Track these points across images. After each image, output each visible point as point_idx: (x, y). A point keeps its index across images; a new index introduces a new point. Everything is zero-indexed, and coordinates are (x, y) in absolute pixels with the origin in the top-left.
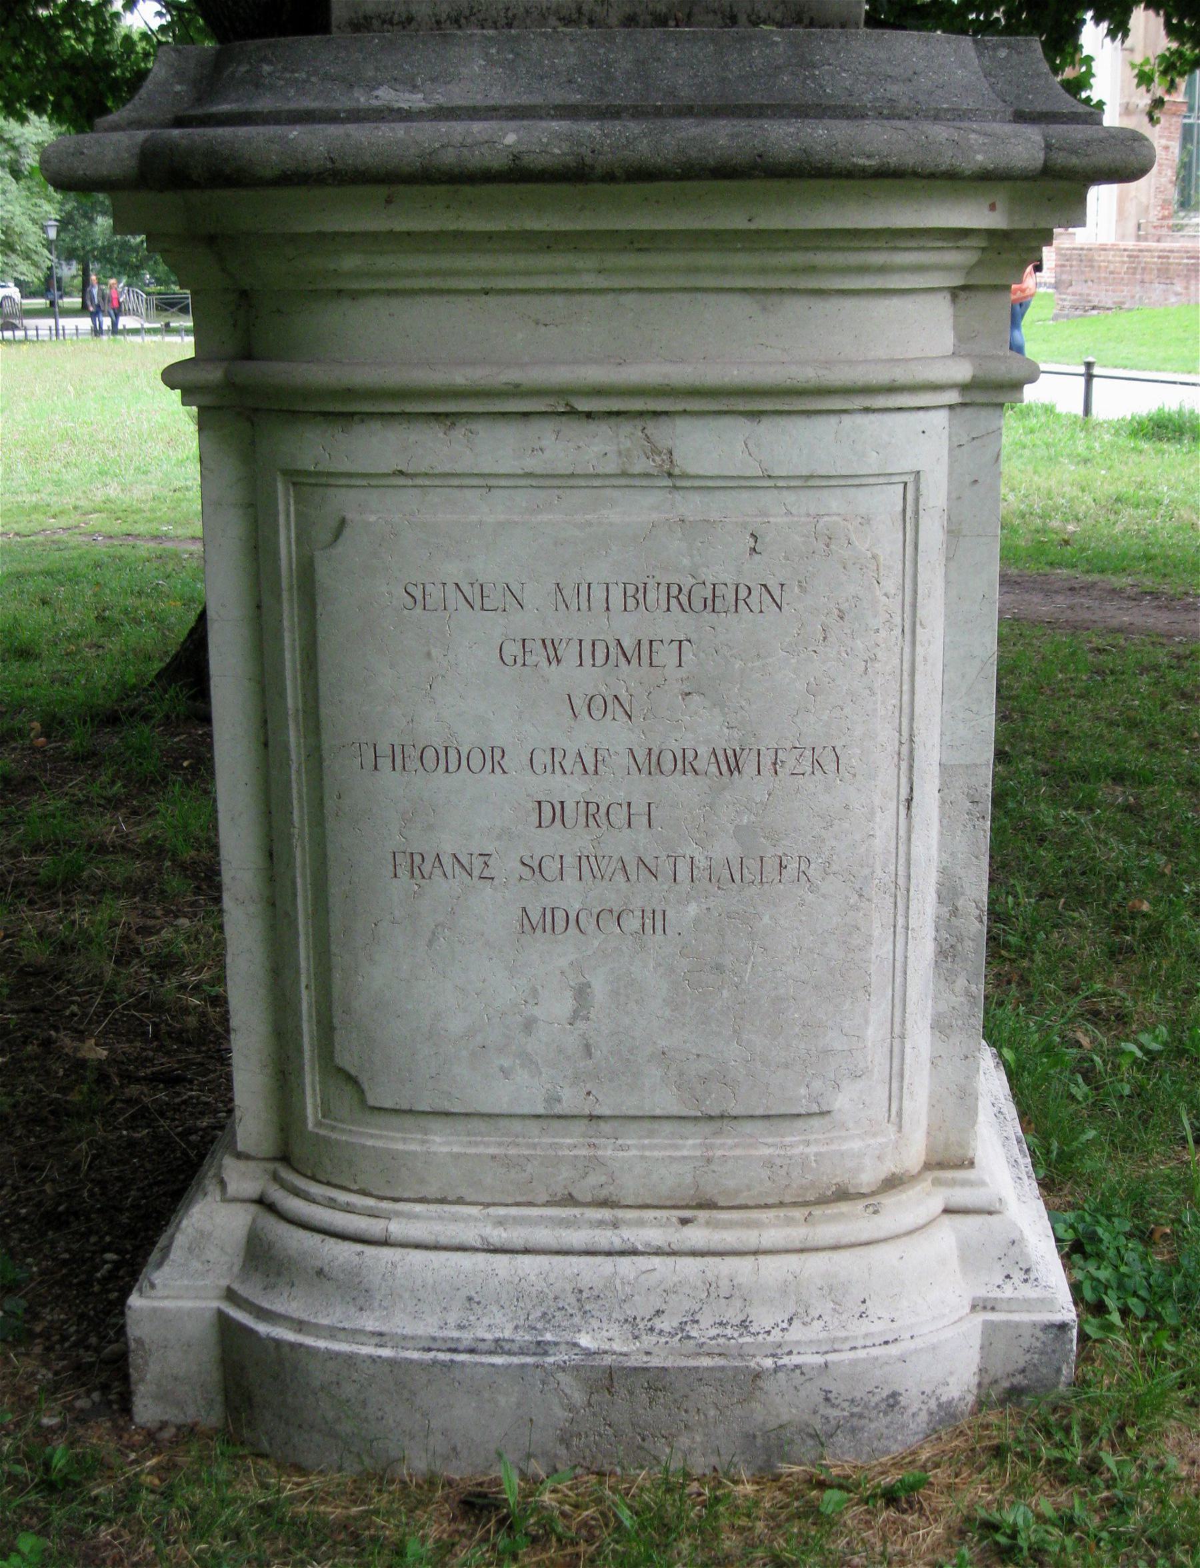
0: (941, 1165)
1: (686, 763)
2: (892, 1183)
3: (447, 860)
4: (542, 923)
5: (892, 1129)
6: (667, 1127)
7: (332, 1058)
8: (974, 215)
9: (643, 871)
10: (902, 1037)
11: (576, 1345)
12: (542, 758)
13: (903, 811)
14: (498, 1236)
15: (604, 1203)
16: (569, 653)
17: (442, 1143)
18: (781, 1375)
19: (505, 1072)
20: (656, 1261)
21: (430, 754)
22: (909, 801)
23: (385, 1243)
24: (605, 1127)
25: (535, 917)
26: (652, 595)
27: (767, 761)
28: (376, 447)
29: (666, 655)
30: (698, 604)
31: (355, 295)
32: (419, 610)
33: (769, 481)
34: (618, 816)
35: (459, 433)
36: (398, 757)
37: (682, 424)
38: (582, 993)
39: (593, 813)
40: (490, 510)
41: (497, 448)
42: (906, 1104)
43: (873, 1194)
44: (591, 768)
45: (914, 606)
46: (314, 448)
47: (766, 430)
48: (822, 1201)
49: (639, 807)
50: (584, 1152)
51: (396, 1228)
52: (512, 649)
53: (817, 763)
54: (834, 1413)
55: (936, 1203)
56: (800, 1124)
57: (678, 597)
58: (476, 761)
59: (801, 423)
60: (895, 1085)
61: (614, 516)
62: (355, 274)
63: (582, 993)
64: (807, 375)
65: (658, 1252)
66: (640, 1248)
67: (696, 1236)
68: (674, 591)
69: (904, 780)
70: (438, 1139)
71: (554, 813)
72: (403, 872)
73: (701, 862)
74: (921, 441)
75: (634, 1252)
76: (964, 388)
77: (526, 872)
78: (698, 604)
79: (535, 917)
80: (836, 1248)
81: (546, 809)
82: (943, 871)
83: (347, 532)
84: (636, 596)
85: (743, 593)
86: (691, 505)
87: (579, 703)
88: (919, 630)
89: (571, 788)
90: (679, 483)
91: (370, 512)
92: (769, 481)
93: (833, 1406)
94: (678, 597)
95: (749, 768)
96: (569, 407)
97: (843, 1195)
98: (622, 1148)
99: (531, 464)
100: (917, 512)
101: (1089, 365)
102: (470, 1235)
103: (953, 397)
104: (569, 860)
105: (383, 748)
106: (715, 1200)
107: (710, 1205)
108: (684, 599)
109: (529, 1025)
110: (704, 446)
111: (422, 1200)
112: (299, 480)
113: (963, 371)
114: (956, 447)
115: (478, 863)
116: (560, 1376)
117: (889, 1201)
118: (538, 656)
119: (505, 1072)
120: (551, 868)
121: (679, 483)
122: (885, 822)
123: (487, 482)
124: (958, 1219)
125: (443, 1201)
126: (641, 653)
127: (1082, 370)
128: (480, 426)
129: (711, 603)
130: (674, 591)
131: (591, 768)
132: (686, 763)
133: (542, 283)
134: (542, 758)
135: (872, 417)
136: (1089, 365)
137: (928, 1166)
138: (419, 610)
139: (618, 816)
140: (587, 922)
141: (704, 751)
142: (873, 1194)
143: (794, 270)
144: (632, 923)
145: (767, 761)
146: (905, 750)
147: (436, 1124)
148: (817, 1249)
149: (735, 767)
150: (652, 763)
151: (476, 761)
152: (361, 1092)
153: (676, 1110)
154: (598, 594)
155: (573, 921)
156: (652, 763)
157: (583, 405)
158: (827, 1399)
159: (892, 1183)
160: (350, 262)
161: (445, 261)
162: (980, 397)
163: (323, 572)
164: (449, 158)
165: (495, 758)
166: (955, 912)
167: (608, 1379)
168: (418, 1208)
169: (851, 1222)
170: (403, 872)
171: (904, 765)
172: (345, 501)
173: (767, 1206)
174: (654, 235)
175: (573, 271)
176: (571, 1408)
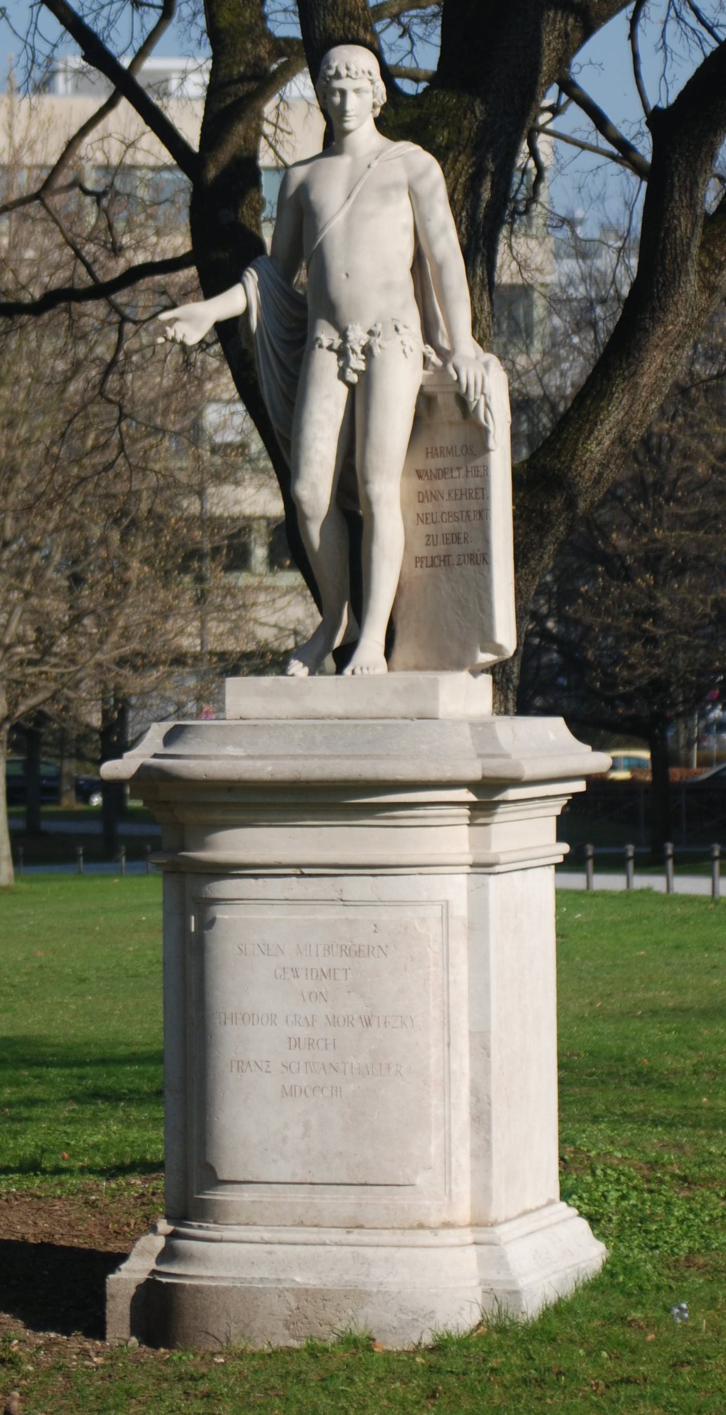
0: (477, 1225)
1: (348, 1021)
2: (447, 1225)
3: (252, 1063)
4: (288, 1092)
5: (446, 1199)
9: (332, 1070)
10: (450, 1154)
11: (294, 1281)
12: (291, 1019)
13: (446, 1048)
14: (267, 1236)
15: (316, 1226)
16: (302, 973)
18: (380, 1296)
19: (275, 1161)
20: (334, 1248)
21: (246, 1017)
22: (449, 1044)
23: (221, 1241)
25: (288, 1089)
26: (335, 949)
27: (382, 1021)
29: (340, 975)
30: (353, 953)
32: (243, 956)
34: (322, 1044)
38: (307, 1126)
39: (311, 1043)
40: (271, 914)
42: (453, 1187)
43: (436, 1228)
44: (310, 1023)
45: (448, 958)
48: (411, 1228)
49: (330, 1041)
50: (308, 1201)
52: (279, 972)
53: (403, 1023)
54: (404, 1317)
55: (470, 1239)
57: (346, 951)
58: (265, 1020)
60: (447, 1178)
61: (319, 917)
63: (307, 1126)
64: (393, 860)
65: (336, 1244)
66: (328, 1242)
67: (355, 1236)
68: (344, 948)
69: (446, 1034)
70: (247, 1195)
71: (294, 1043)
72: (235, 1069)
73: (356, 1066)
74: (456, 888)
75: (325, 1244)
76: (472, 866)
77: (284, 1069)
78: (353, 953)
79: (288, 1089)
80: (412, 1247)
81: (292, 1040)
82: (472, 1081)
84: (328, 949)
85: (371, 949)
86: (350, 913)
87: (306, 995)
88: (451, 969)
89: (302, 1032)
90: (346, 903)
91: (222, 914)
93: (404, 1313)
94: (346, 951)
97: (421, 1226)
98: (324, 1199)
100: (447, 918)
102: (256, 1236)
104: (302, 1064)
106: (364, 1224)
107: (361, 1227)
108: (347, 951)
110: (356, 887)
111: (239, 1224)
113: (470, 859)
114: (470, 891)
115: (265, 1064)
116: (286, 1293)
117: (443, 1233)
118: (289, 975)
119: (275, 1161)
120: (294, 1067)
121: (346, 903)
122: (435, 1053)
124: (479, 1247)
125: (247, 1224)
126: (328, 974)
129: (358, 953)
130: (344, 948)
131: (310, 1023)
132: (348, 1021)
134: (291, 1019)
135: (423, 877)
137: (471, 1225)
138: (243, 956)
139: (322, 1044)
140: (309, 1092)
141: (356, 1016)
142: (436, 1228)
144: (327, 1092)
145: (382, 1021)
146: (446, 1021)
148: (406, 1246)
149: (368, 1024)
150: (334, 1021)
151: (265, 1020)
154: (313, 948)
155: (303, 1092)
156: (334, 1021)
157: (306, 871)
158: (401, 1310)
159: (447, 1225)
166: (478, 1100)
167: (303, 1293)
168: (236, 1227)
169: (425, 1237)
170: (235, 1069)
171: (446, 1028)
173: (386, 1228)
176: (291, 1311)
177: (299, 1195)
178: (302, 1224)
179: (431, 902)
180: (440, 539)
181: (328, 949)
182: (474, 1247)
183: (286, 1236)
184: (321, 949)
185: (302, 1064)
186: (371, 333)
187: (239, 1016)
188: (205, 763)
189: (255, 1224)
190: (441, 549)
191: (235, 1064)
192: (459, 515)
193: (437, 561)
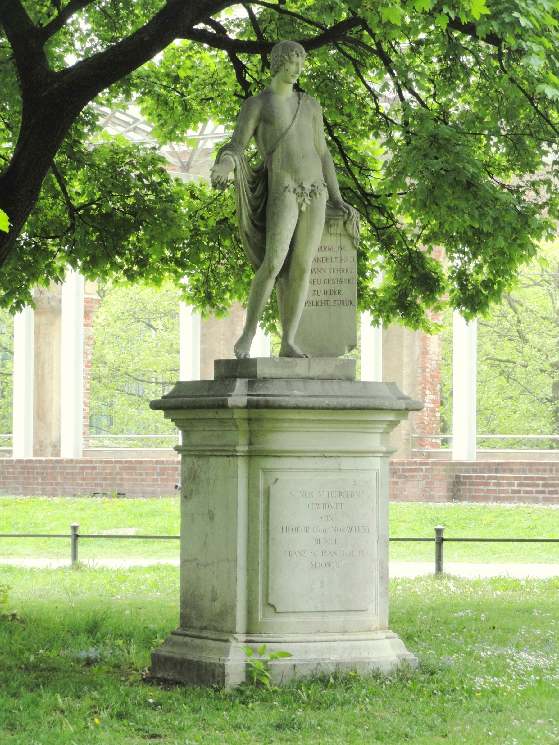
4: (315, 566)
6: (337, 613)
7: (267, 600)
8: (391, 417)
17: (292, 619)
21: (294, 529)
24: (325, 614)
28: (285, 463)
31: (283, 431)
33: (357, 471)
34: (330, 542)
35: (302, 460)
36: (287, 530)
37: (342, 459)
38: (322, 582)
41: (308, 463)
46: (269, 463)
47: (357, 460)
51: (287, 639)
52: (311, 506)
53: (365, 530)
55: (384, 636)
56: (362, 612)
57: (342, 494)
59: (362, 459)
62: (286, 427)
63: (322, 582)
67: (346, 637)
71: (317, 541)
75: (335, 641)
83: (278, 481)
91: (283, 477)
92: (357, 471)
94: (342, 494)
95: (354, 531)
96: (324, 455)
97: (370, 630)
99: (315, 467)
101: (75, 528)
103: (381, 455)
104: (321, 552)
105: (285, 528)
107: (347, 632)
109: (312, 589)
110: (347, 463)
112: (265, 470)
120: (317, 553)
123: (306, 470)
127: (70, 532)
128: (306, 459)
129: (347, 496)
133: (319, 430)
136: (75, 528)
143: (363, 428)
144: (332, 565)
147: (291, 615)
149: (351, 531)
152: (275, 608)
153: (340, 609)
154: (327, 493)
160: (286, 425)
161: (303, 425)
162: (386, 455)
163: (272, 490)
164: (316, 405)
165: (307, 529)
166: (383, 568)
172: (277, 475)
174: (342, 420)
175: (325, 427)
177: (317, 618)
178: (319, 632)
179: (369, 471)
180: (322, 292)
181: (334, 494)
182: (387, 640)
183: (317, 638)
184: (330, 493)
185: (321, 552)
186: (313, 186)
187: (291, 528)
188: (288, 399)
189: (297, 633)
190: (323, 298)
191: (288, 553)
192: (336, 281)
193: (320, 304)
